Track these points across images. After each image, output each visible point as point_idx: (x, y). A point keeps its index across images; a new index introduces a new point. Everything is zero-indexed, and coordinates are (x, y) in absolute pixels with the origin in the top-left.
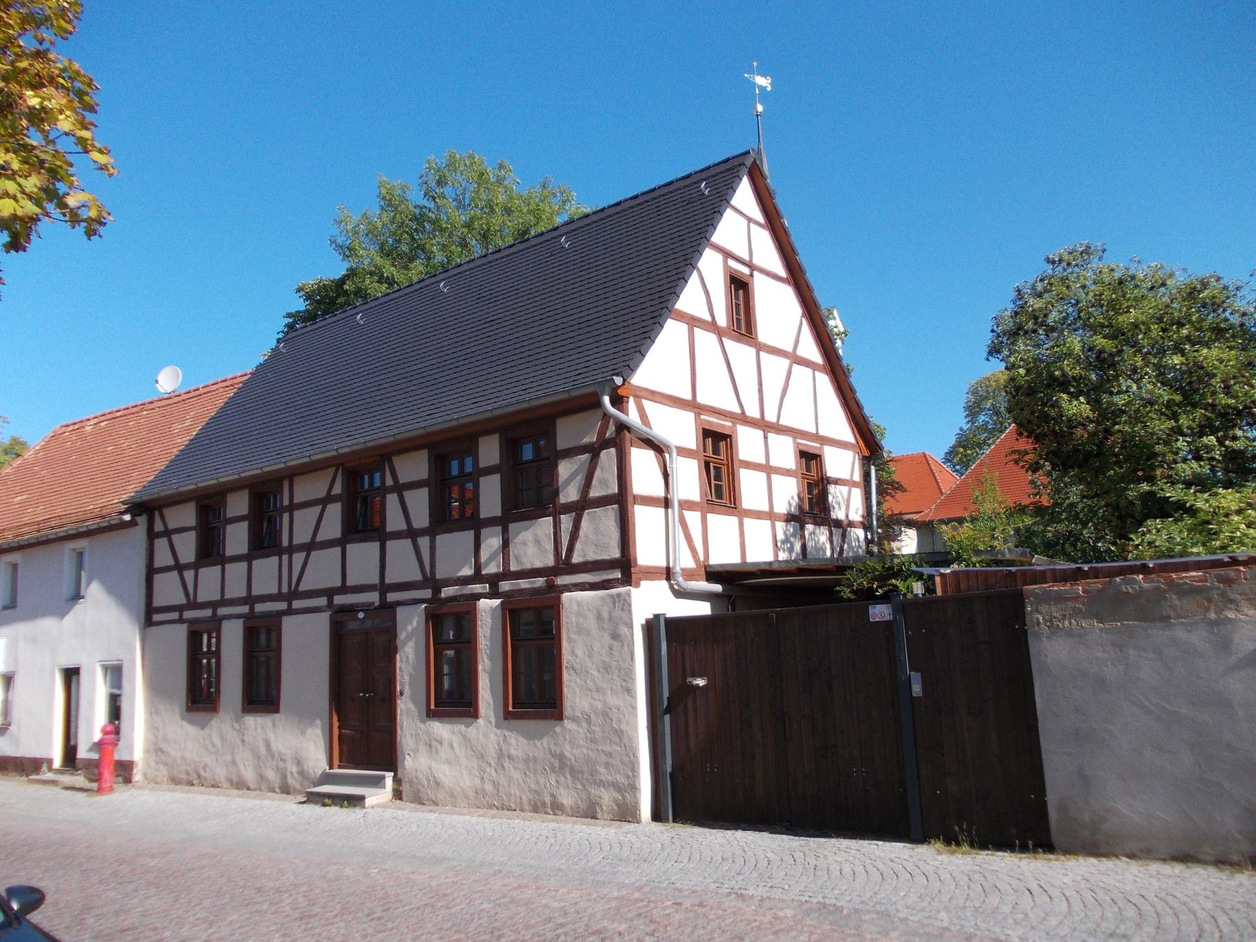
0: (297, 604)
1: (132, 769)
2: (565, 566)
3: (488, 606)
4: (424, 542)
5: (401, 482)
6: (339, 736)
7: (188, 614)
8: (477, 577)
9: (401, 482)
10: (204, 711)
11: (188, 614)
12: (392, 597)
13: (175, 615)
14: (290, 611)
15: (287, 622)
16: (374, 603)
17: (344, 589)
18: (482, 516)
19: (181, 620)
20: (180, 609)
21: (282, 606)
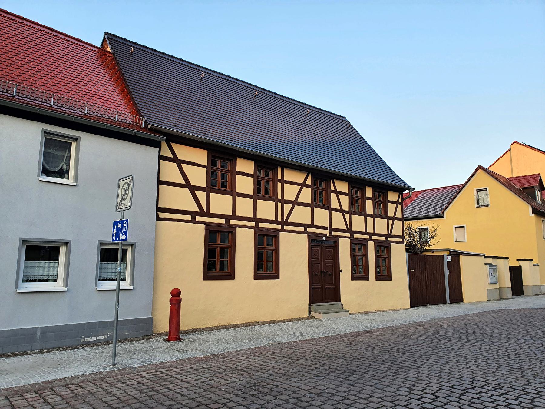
0: (286, 228)
1: (49, 259)
2: (389, 235)
3: (371, 245)
4: (390, 221)
5: (211, 212)
6: (114, 331)
7: (309, 230)
8: (365, 233)
9: (211, 212)
10: (173, 135)
11: (309, 230)
12: (390, 239)
13: (302, 229)
14: (283, 230)
15: (281, 233)
16: (327, 235)
17: (312, 226)
18: (252, 216)
19: (305, 232)
20: (306, 226)
21: (279, 227)
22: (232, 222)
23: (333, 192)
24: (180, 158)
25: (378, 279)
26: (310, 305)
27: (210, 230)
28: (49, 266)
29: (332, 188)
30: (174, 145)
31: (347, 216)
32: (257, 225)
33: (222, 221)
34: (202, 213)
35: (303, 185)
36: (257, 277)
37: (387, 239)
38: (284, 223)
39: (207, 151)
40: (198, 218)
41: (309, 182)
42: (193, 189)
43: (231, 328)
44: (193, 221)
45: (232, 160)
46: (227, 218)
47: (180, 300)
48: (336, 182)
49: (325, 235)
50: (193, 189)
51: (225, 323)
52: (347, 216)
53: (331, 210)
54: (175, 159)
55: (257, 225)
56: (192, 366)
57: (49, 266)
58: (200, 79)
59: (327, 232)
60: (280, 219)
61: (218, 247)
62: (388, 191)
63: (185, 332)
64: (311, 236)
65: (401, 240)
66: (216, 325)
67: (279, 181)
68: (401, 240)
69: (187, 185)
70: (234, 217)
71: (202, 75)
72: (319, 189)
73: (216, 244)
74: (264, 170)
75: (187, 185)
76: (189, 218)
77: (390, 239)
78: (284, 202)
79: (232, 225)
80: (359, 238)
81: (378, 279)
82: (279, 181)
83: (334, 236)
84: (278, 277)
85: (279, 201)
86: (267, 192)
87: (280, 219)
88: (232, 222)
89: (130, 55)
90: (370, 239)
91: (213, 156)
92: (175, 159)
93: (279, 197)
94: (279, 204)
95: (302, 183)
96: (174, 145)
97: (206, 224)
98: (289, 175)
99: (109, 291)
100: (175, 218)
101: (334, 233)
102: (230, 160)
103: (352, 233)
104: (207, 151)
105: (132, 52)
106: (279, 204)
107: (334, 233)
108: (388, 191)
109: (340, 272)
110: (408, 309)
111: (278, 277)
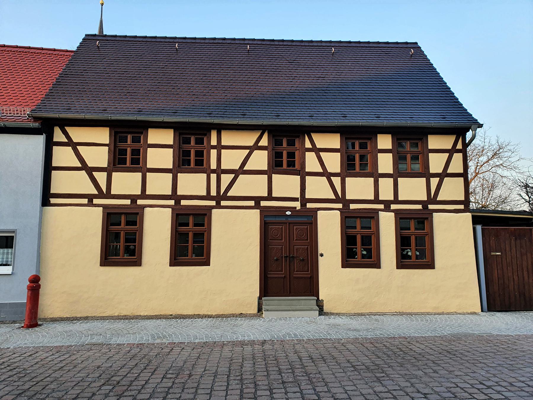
0: (223, 203)
1: (7, 247)
7: (263, 203)
12: (431, 207)
13: (252, 203)
14: (218, 206)
16: (296, 208)
20: (258, 200)
21: (213, 203)
22: (140, 202)
23: (309, 150)
24: (75, 140)
25: (400, 265)
26: (260, 298)
27: (108, 213)
28: (8, 253)
29: (308, 145)
30: (68, 129)
31: (337, 181)
32: (178, 202)
33: (128, 202)
34: (101, 195)
35: (256, 147)
36: (345, 264)
37: (425, 207)
38: (220, 198)
39: (390, 136)
40: (96, 201)
41: (264, 142)
42: (90, 171)
43: (147, 319)
44: (91, 204)
45: (423, 138)
46: (133, 198)
47: (39, 286)
48: (314, 136)
49: (293, 209)
50: (90, 171)
51: (124, 313)
52: (337, 181)
53: (303, 174)
54: (70, 143)
55: (178, 202)
56: (516, 347)
57: (8, 253)
58: (410, 57)
59: (297, 205)
60: (213, 193)
61: (358, 234)
62: (429, 136)
63: (45, 320)
64: (265, 213)
65: (462, 207)
66: (116, 314)
67: (214, 147)
68: (462, 207)
69: (84, 167)
70: (144, 195)
71: (411, 52)
72: (129, 147)
73: (120, 227)
74: (408, 142)
75: (84, 167)
76: (85, 201)
77: (431, 207)
78: (220, 171)
79: (140, 205)
80: (360, 209)
81: (400, 265)
82: (214, 147)
83: (308, 208)
84: (208, 264)
85: (214, 171)
86: (291, 164)
87: (213, 193)
88: (140, 202)
89: (331, 56)
90: (387, 209)
91: (398, 139)
92: (70, 143)
93: (214, 166)
94: (214, 176)
95: (450, 148)
96: (68, 129)
97: (105, 207)
98: (228, 138)
99: (6, 276)
100: (69, 203)
101: (309, 205)
102: (421, 139)
103: (346, 203)
104: (390, 136)
105: (412, 54)
106: (214, 176)
107: (309, 205)
108: (429, 136)
109: (320, 257)
110: (474, 313)
111: (208, 264)
